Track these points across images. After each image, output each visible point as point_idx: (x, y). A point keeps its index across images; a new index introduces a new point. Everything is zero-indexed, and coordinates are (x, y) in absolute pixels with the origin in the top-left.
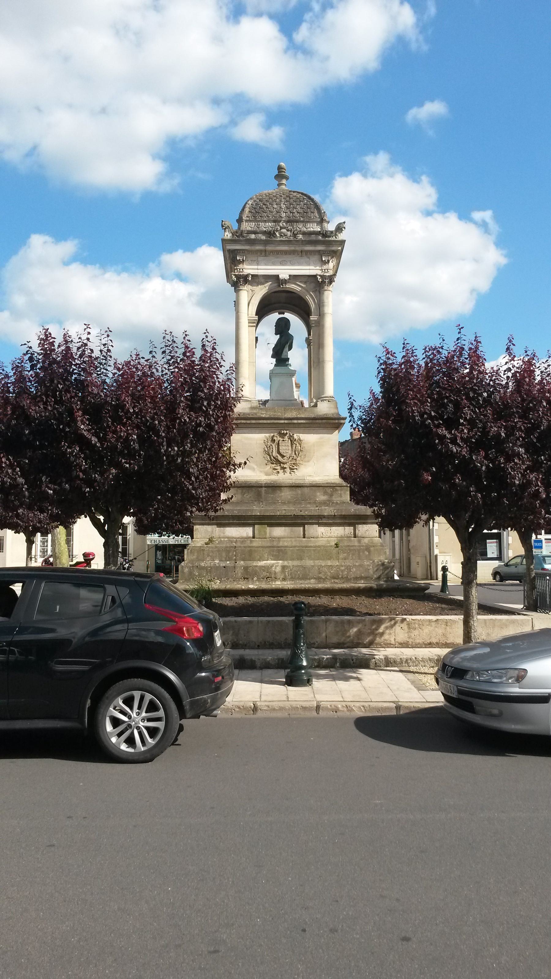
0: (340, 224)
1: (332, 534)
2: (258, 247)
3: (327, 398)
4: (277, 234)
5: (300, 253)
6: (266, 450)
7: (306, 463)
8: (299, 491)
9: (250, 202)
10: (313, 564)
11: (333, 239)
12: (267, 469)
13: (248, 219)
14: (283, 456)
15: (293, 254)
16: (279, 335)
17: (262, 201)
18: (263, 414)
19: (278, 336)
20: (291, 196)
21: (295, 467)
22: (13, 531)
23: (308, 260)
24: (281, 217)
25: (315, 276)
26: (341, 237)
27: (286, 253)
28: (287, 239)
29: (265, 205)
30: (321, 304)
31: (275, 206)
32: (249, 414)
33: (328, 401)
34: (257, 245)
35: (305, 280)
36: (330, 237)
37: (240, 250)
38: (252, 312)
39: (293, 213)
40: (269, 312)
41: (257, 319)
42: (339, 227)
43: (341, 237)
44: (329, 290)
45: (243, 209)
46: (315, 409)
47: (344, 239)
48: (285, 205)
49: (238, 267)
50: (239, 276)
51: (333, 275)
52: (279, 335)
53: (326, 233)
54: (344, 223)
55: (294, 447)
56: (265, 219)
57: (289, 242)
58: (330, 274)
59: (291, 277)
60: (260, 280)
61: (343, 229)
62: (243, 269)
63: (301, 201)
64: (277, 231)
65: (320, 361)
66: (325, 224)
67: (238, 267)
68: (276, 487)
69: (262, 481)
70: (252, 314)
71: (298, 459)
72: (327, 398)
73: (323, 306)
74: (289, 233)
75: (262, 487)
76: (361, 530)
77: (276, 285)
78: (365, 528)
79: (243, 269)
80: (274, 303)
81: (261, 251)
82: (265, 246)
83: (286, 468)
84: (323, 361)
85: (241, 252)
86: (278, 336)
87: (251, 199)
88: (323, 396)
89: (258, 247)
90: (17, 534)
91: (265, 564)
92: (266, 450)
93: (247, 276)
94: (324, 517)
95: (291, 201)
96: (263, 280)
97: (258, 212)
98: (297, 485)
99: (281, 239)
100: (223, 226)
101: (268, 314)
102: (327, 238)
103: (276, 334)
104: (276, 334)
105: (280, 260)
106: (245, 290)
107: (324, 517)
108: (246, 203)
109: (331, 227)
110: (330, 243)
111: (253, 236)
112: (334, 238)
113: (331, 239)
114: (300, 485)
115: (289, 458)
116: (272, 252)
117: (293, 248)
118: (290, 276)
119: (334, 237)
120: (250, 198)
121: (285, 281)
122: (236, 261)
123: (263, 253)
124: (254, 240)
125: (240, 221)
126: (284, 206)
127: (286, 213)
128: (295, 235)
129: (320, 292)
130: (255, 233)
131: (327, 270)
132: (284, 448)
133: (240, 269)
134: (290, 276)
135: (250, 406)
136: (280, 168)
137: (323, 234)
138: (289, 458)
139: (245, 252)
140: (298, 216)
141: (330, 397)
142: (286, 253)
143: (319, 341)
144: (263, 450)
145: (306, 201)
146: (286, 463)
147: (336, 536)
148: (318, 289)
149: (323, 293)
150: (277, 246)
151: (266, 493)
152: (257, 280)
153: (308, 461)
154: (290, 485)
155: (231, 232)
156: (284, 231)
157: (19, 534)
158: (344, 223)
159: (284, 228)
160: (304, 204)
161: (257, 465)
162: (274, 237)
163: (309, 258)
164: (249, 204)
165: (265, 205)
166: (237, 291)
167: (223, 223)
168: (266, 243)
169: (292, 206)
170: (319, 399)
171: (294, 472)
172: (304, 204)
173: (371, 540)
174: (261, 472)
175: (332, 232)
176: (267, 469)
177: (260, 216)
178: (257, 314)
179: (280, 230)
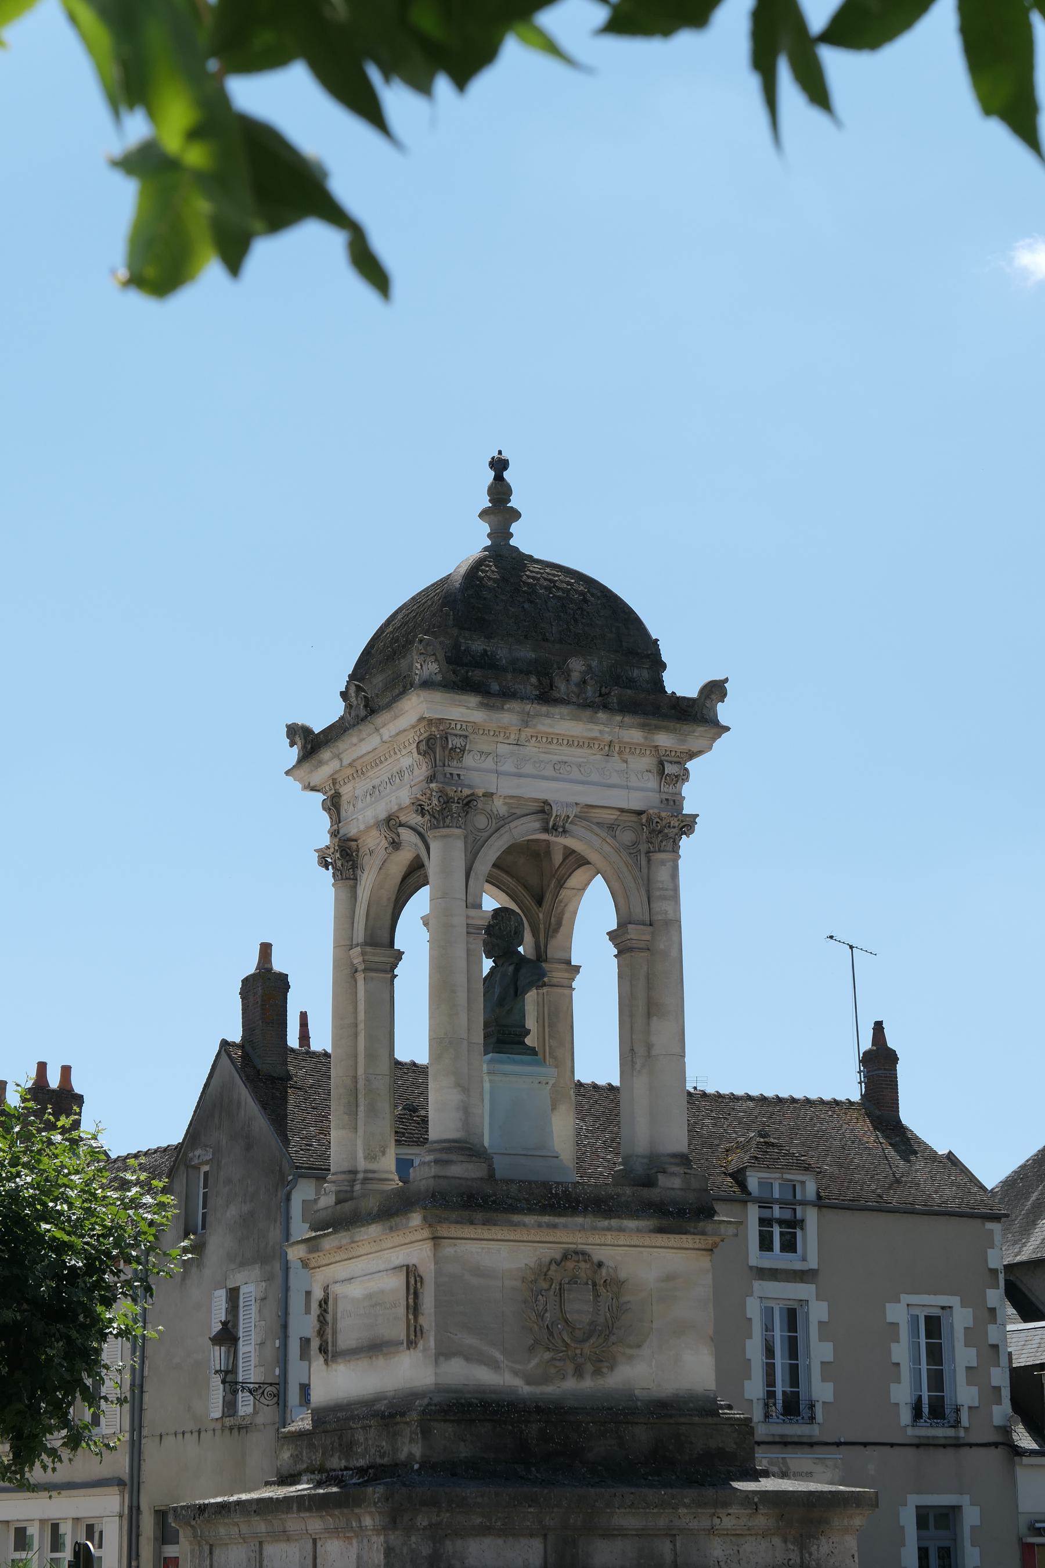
54: (726, 680)
153: (639, 1346)
158: (726, 680)
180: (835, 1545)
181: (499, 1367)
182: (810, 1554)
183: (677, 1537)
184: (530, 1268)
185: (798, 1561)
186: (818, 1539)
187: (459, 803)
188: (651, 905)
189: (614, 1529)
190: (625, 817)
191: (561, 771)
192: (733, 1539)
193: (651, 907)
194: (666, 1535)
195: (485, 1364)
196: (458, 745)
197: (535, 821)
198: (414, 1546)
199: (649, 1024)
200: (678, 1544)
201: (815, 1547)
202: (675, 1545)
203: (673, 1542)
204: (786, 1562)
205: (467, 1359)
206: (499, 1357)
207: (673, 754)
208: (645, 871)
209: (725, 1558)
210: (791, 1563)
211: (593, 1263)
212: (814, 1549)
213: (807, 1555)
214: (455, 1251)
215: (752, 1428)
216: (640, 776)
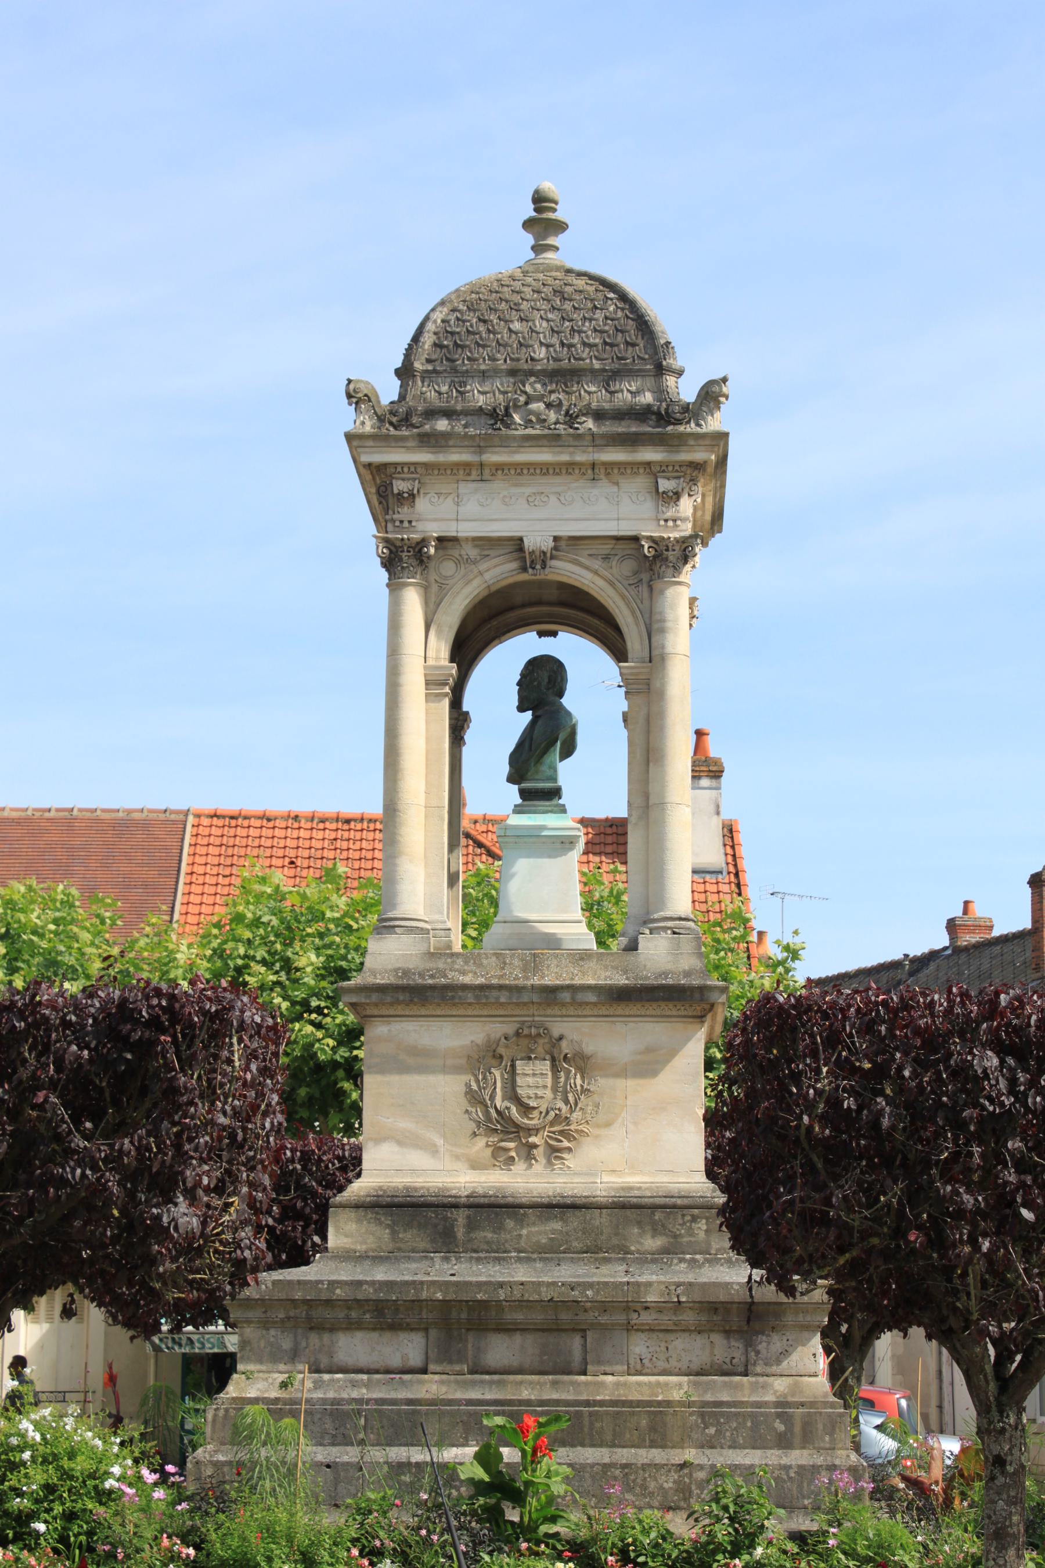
0: (711, 383)
1: (673, 1363)
2: (456, 456)
3: (670, 924)
4: (517, 418)
5: (590, 472)
6: (475, 1087)
7: (603, 1132)
8: (575, 1220)
9: (438, 316)
10: (607, 1460)
11: (689, 430)
12: (476, 1148)
13: (430, 367)
14: (526, 1109)
15: (568, 473)
16: (530, 712)
17: (475, 311)
18: (464, 973)
19: (528, 716)
20: (568, 289)
21: (566, 1144)
22: (911, 956)
23: (615, 489)
24: (532, 359)
25: (636, 539)
26: (714, 423)
27: (545, 470)
28: (546, 432)
29: (485, 321)
30: (655, 626)
31: (516, 326)
32: (421, 975)
33: (674, 933)
34: (454, 450)
35: (606, 548)
36: (678, 422)
37: (403, 465)
38: (438, 651)
39: (570, 346)
40: (504, 634)
41: (454, 672)
42: (707, 392)
43: (714, 423)
44: (679, 583)
45: (416, 338)
46: (631, 957)
47: (725, 429)
48: (548, 321)
49: (395, 516)
50: (399, 544)
51: (691, 537)
52: (530, 712)
53: (667, 410)
54: (724, 380)
55: (562, 1080)
56: (483, 367)
57: (554, 440)
58: (683, 534)
59: (563, 543)
60: (463, 553)
61: (722, 399)
62: (410, 522)
63: (596, 308)
64: (516, 407)
65: (651, 802)
66: (670, 381)
67: (395, 516)
68: (500, 1206)
69: (459, 1189)
70: (437, 659)
71: (576, 1115)
72: (670, 924)
73: (662, 631)
74: (552, 416)
75: (456, 1206)
76: (764, 1352)
77: (514, 565)
78: (778, 1344)
79: (410, 522)
80: (524, 606)
81: (467, 466)
82: (481, 453)
83: (535, 1146)
84: (662, 805)
85: (406, 470)
86: (528, 716)
87: (442, 303)
88: (656, 916)
89: (456, 456)
90: (567, 807)
91: (456, 1456)
92: (475, 1087)
93: (423, 542)
94: (647, 1308)
95: (568, 306)
96: (473, 553)
97: (463, 347)
98: (569, 1201)
99: (530, 431)
100: (349, 396)
101: (503, 638)
102: (670, 428)
103: (521, 709)
104: (521, 709)
105: (528, 491)
106: (411, 584)
107: (647, 1308)
108: (427, 318)
109: (687, 390)
110: (682, 440)
111: (442, 425)
112: (692, 428)
113: (681, 428)
114: (579, 1201)
115: (547, 1113)
116: (500, 467)
117: (565, 458)
118: (556, 539)
119: (693, 425)
120: (438, 300)
121: (543, 559)
122: (390, 496)
123: (474, 473)
124: (446, 436)
125: (404, 372)
126: (545, 324)
127: (548, 346)
128: (571, 419)
129: (651, 588)
130: (448, 414)
131: (675, 521)
132: (530, 1080)
133: (402, 522)
134: (556, 539)
135: (422, 948)
136: (540, 200)
137: (658, 414)
138: (547, 1113)
139: (419, 470)
140: (585, 355)
141: (680, 919)
142: (545, 470)
143: (648, 743)
144: (464, 1089)
145: (611, 309)
146: (538, 1130)
147: (684, 1368)
148: (645, 577)
149: (662, 592)
150: (519, 452)
151: (471, 1226)
152: (455, 553)
153: (608, 1125)
154: (545, 1200)
155: (375, 413)
156: (538, 406)
157: (511, 779)
158: (724, 380)
159: (540, 398)
160: (606, 318)
161: (444, 1136)
162: (508, 426)
163: (617, 484)
164: (435, 322)
165: (485, 321)
166: (395, 586)
167: (352, 387)
168: (480, 445)
169: (567, 323)
170: (645, 923)
171: (563, 1158)
172: (606, 318)
173: (796, 1384)
174: (457, 1158)
175: (686, 408)
176: (476, 1148)
177: (469, 359)
178: (452, 660)
179: (527, 403)
180: (790, 1342)
181: (437, 1151)
182: (758, 1353)
183: (588, 1332)
184: (477, 1045)
185: (743, 1359)
186: (769, 1335)
187: (409, 551)
188: (653, 640)
189: (510, 1323)
190: (622, 545)
191: (536, 503)
192: (661, 1335)
193: (654, 644)
194: (574, 1330)
195: (421, 1149)
196: (405, 490)
197: (511, 561)
198: (272, 1339)
199: (648, 772)
200: (588, 1340)
201: (764, 1344)
202: (586, 1340)
203: (584, 1337)
204: (728, 1360)
205: (400, 1143)
206: (440, 1142)
207: (670, 468)
208: (647, 602)
209: (649, 1356)
210: (734, 1361)
211: (551, 1037)
212: (762, 1347)
213: (753, 1354)
214: (389, 1031)
215: (323, 1209)
216: (634, 498)
